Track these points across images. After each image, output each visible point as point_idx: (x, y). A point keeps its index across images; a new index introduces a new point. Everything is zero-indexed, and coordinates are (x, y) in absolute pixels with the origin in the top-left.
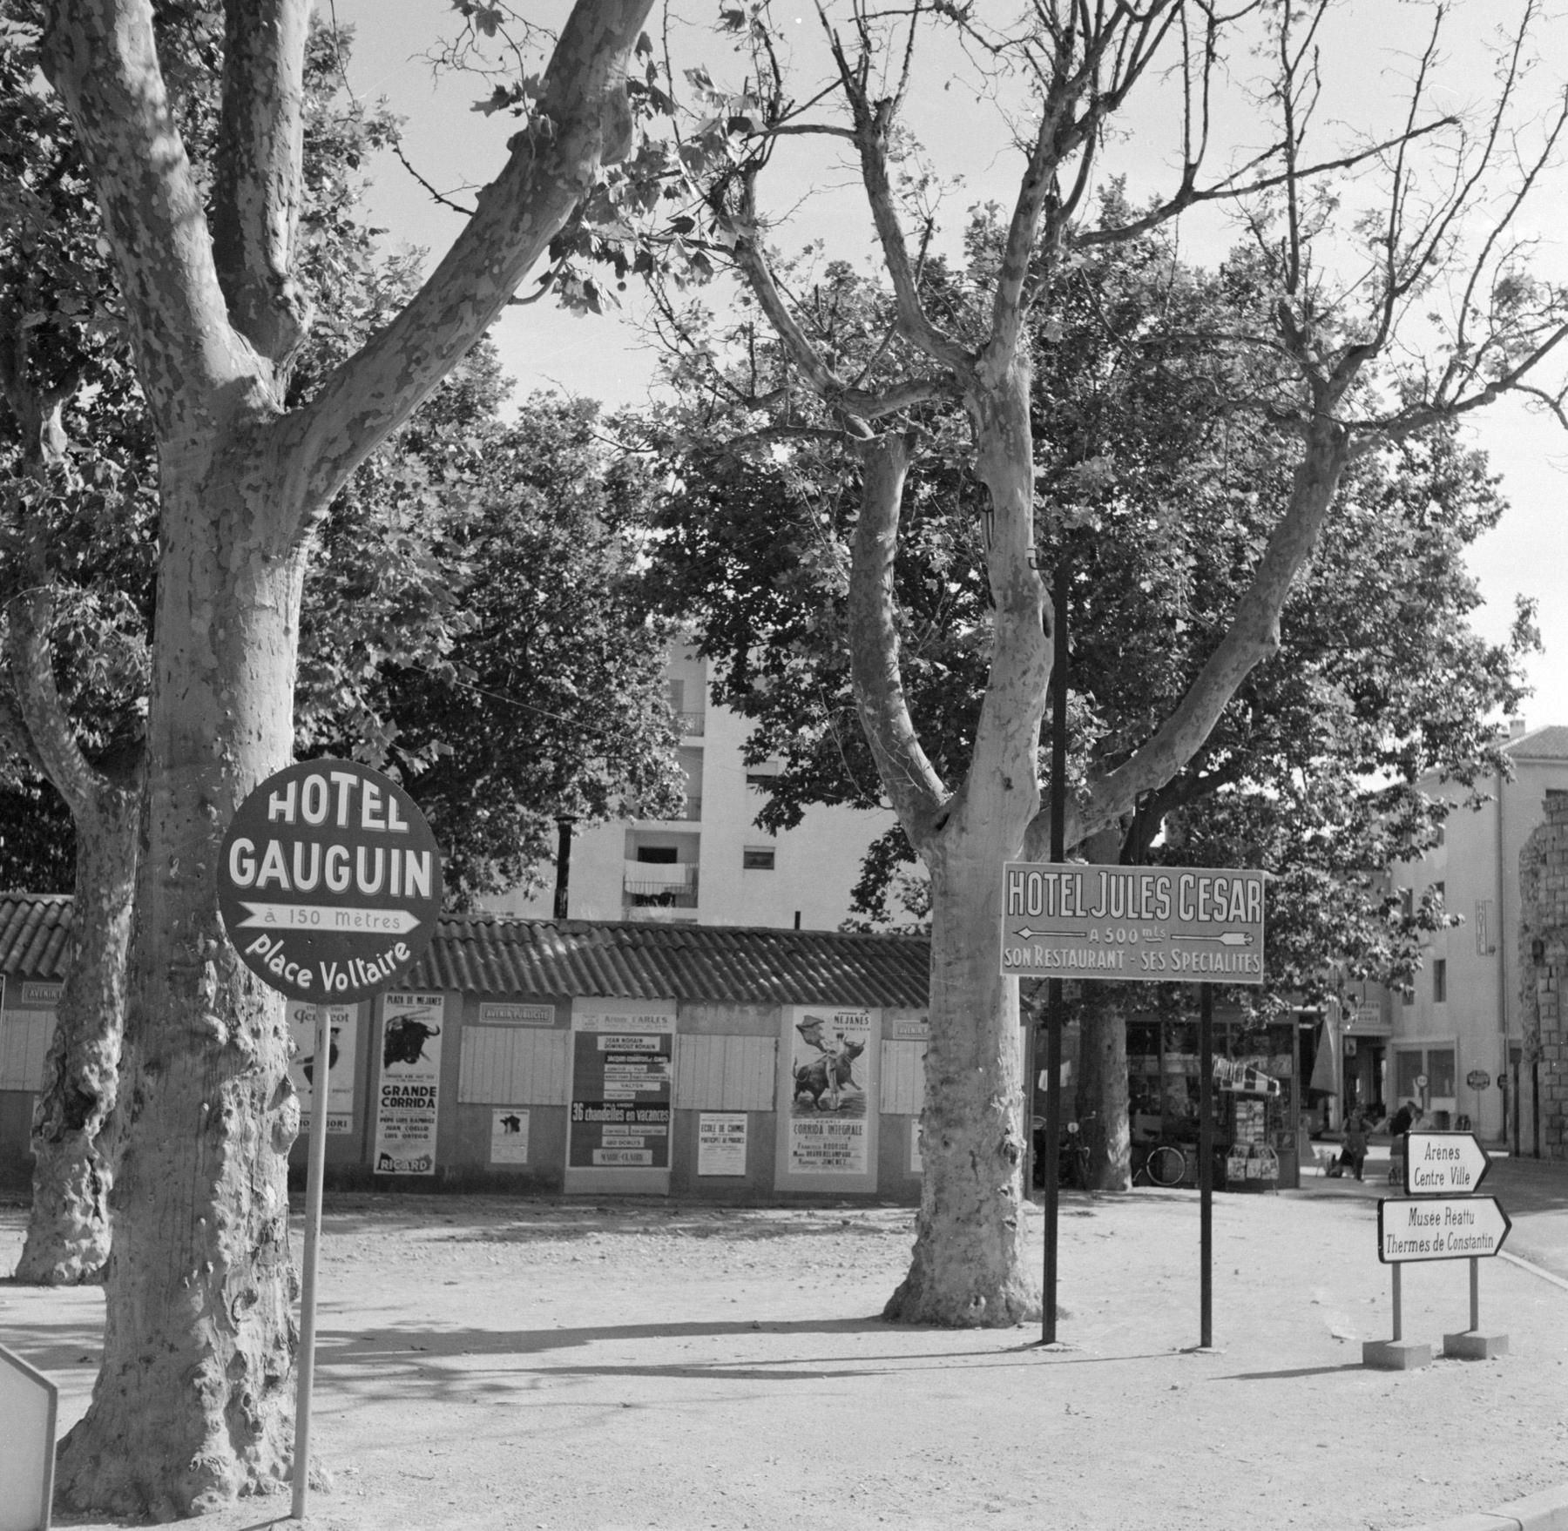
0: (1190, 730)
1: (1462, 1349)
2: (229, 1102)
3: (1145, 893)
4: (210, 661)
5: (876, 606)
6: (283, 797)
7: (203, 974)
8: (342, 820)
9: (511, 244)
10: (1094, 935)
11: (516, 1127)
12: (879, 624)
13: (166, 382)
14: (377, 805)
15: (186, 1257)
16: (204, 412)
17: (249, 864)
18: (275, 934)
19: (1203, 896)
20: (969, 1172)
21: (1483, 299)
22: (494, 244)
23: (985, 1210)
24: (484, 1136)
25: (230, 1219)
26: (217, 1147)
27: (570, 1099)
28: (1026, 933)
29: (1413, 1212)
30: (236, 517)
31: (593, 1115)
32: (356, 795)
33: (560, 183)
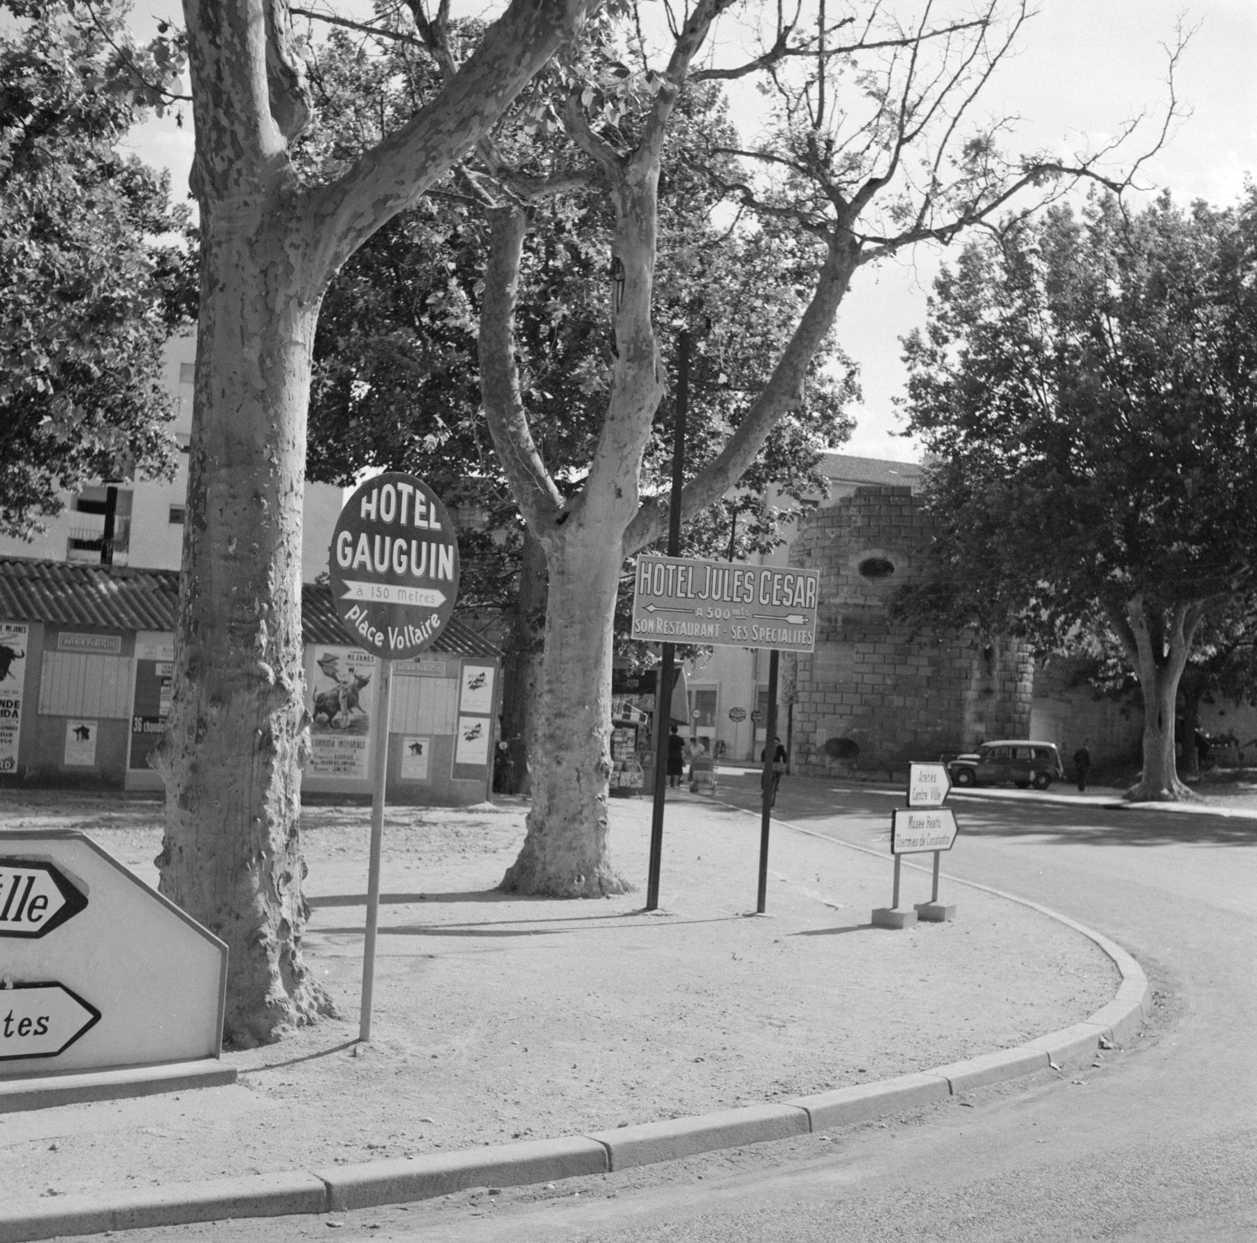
0: (740, 460)
1: (930, 914)
2: (275, 729)
3: (737, 583)
4: (259, 384)
5: (503, 344)
6: (369, 501)
7: (258, 629)
8: (403, 520)
9: (514, 75)
10: (699, 612)
11: (419, 752)
12: (505, 358)
13: (228, 152)
14: (423, 509)
15: (246, 848)
16: (256, 180)
17: (349, 550)
18: (363, 605)
19: (776, 587)
20: (574, 784)
21: (955, 148)
22: (501, 74)
23: (586, 812)
24: (60, 740)
25: (276, 819)
26: (268, 764)
27: (132, 713)
28: (651, 608)
29: (911, 818)
30: (281, 269)
31: (151, 728)
32: (412, 499)
33: (558, 33)
